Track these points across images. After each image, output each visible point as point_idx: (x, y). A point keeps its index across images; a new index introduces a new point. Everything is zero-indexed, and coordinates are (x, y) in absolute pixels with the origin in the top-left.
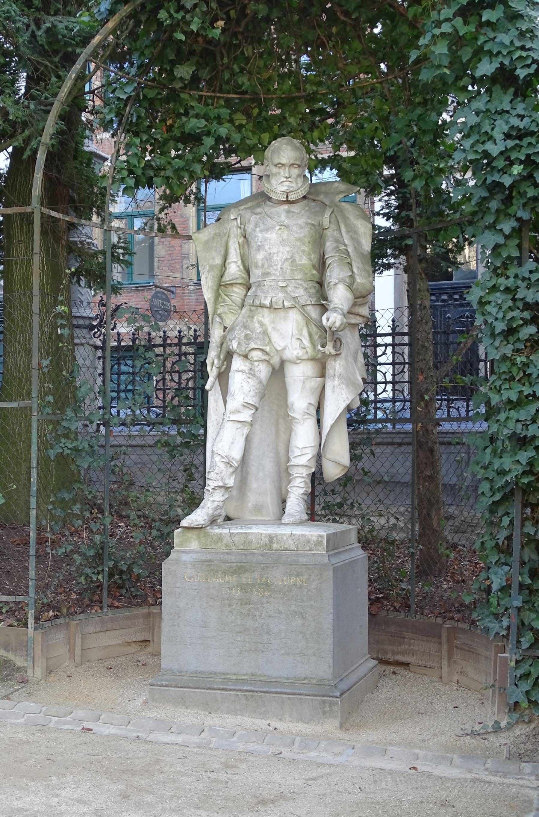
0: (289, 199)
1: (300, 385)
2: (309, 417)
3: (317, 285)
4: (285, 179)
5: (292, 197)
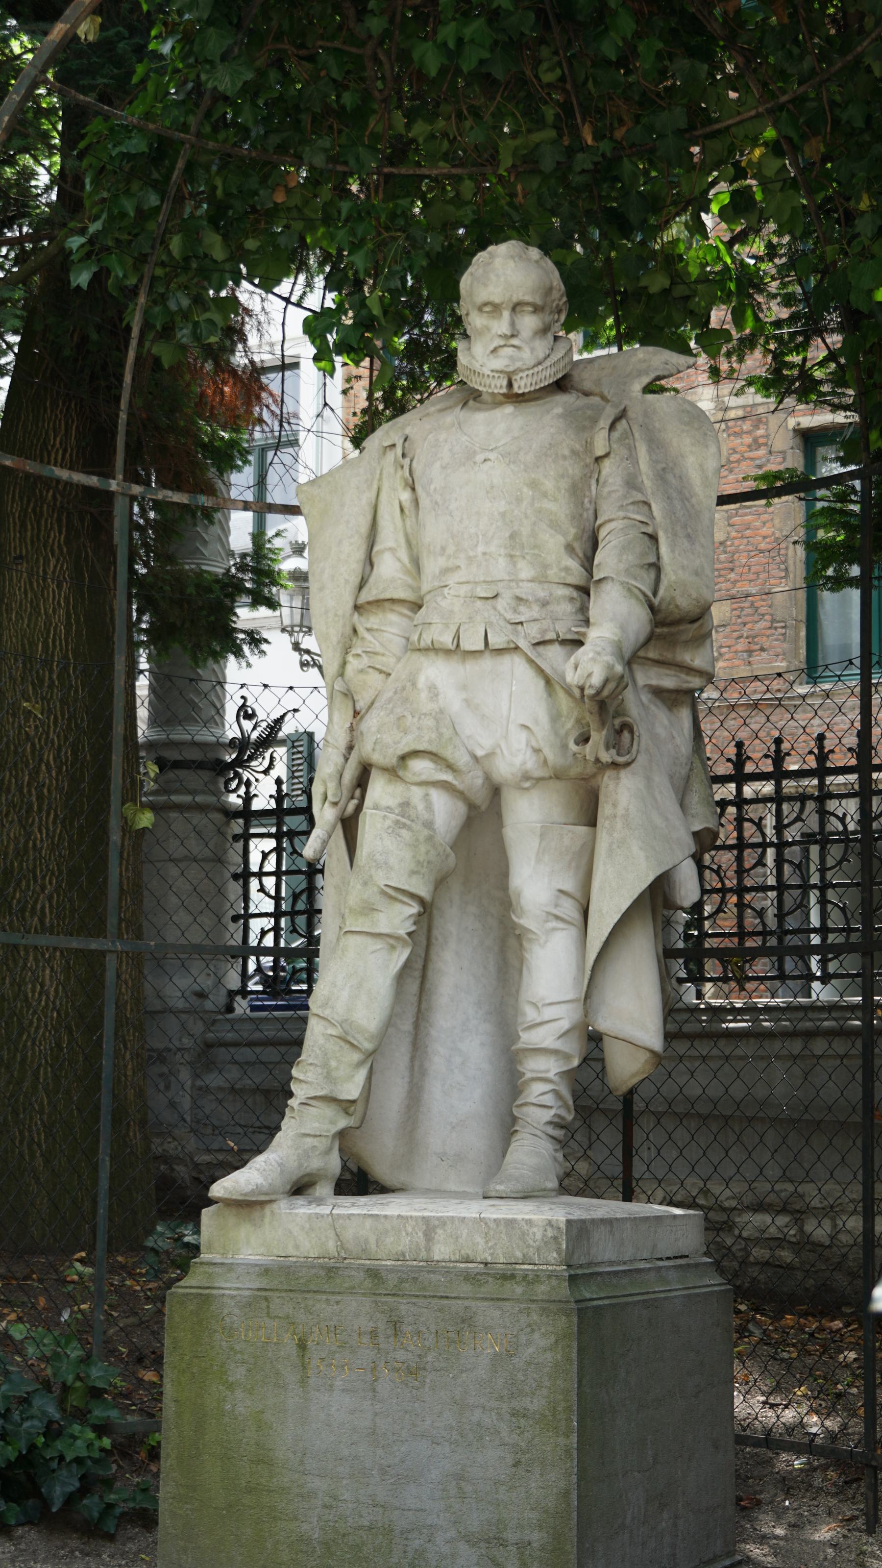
0: (516, 389)
1: (535, 843)
2: (561, 925)
3: (575, 594)
4: (502, 343)
5: (522, 385)
